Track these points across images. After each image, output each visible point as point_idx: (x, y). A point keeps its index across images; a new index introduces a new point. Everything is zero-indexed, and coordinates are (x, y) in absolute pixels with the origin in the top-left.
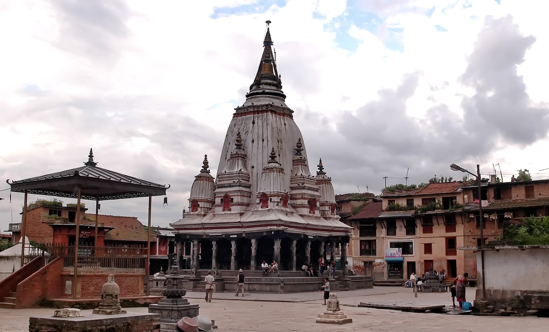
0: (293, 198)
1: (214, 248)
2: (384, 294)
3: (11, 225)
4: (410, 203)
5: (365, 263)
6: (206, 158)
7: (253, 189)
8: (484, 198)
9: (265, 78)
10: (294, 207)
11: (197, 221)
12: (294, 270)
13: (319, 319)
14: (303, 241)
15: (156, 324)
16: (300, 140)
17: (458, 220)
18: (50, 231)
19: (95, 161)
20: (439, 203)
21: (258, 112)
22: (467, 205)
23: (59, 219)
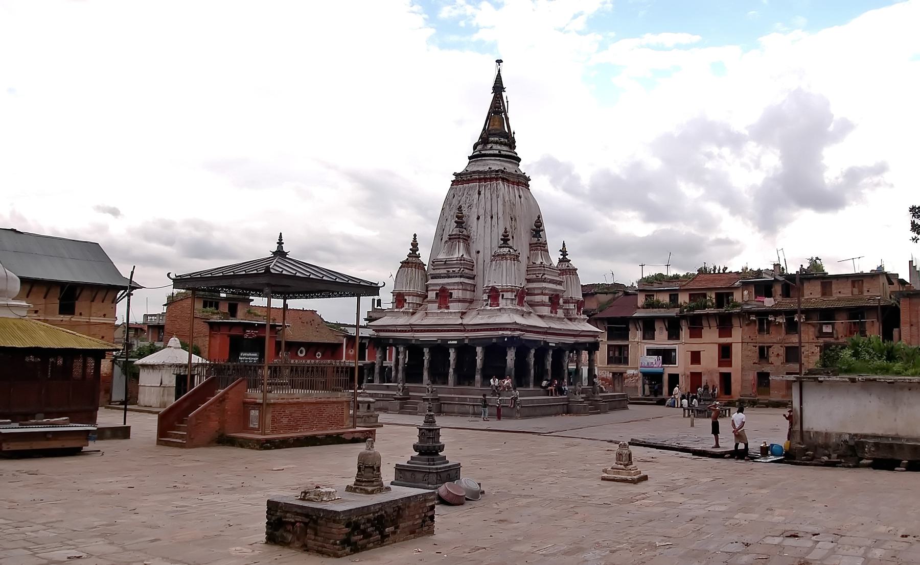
0: (530, 293)
1: (426, 357)
2: (647, 420)
3: (146, 316)
4: (674, 297)
5: (614, 374)
6: (415, 239)
7: (479, 280)
8: (769, 294)
9: (494, 135)
10: (532, 305)
11: (402, 320)
12: (531, 388)
13: (606, 475)
14: (542, 349)
15: (431, 504)
16: (539, 217)
17: (736, 322)
18: (206, 329)
19: (285, 250)
20: (711, 301)
21: (485, 180)
22: (746, 303)
23: (218, 313)
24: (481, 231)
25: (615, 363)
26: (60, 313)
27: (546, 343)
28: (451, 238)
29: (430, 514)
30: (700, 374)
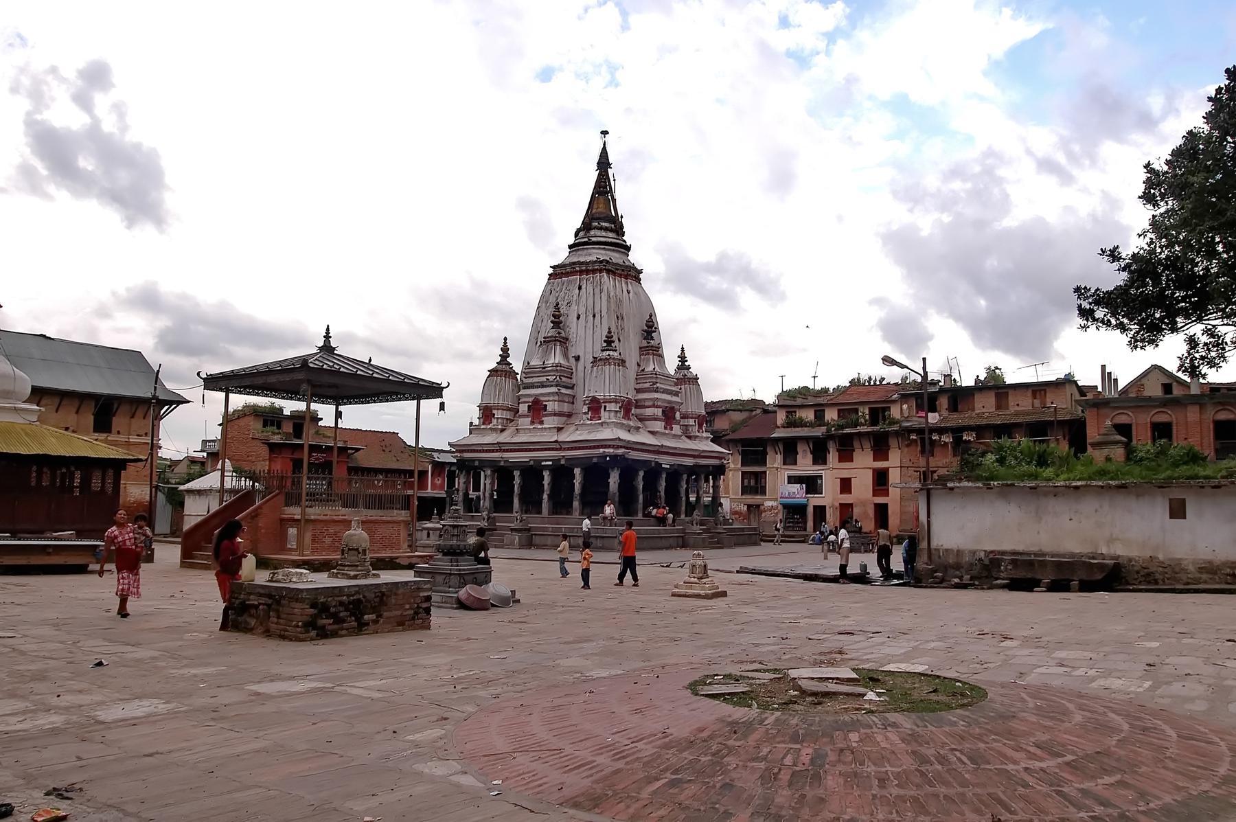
0: (639, 404)
1: (517, 481)
3: (205, 442)
4: (820, 415)
5: (749, 506)
6: (505, 343)
7: (578, 390)
8: (933, 409)
9: (599, 219)
10: (642, 419)
11: (489, 438)
14: (653, 471)
17: (893, 442)
18: (264, 451)
20: (863, 416)
21: (587, 272)
24: (581, 332)
25: (750, 493)
26: (95, 431)
27: (659, 465)
28: (547, 341)
29: (425, 605)
30: (851, 505)
